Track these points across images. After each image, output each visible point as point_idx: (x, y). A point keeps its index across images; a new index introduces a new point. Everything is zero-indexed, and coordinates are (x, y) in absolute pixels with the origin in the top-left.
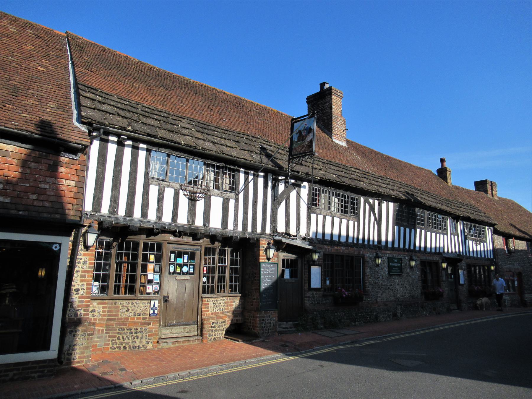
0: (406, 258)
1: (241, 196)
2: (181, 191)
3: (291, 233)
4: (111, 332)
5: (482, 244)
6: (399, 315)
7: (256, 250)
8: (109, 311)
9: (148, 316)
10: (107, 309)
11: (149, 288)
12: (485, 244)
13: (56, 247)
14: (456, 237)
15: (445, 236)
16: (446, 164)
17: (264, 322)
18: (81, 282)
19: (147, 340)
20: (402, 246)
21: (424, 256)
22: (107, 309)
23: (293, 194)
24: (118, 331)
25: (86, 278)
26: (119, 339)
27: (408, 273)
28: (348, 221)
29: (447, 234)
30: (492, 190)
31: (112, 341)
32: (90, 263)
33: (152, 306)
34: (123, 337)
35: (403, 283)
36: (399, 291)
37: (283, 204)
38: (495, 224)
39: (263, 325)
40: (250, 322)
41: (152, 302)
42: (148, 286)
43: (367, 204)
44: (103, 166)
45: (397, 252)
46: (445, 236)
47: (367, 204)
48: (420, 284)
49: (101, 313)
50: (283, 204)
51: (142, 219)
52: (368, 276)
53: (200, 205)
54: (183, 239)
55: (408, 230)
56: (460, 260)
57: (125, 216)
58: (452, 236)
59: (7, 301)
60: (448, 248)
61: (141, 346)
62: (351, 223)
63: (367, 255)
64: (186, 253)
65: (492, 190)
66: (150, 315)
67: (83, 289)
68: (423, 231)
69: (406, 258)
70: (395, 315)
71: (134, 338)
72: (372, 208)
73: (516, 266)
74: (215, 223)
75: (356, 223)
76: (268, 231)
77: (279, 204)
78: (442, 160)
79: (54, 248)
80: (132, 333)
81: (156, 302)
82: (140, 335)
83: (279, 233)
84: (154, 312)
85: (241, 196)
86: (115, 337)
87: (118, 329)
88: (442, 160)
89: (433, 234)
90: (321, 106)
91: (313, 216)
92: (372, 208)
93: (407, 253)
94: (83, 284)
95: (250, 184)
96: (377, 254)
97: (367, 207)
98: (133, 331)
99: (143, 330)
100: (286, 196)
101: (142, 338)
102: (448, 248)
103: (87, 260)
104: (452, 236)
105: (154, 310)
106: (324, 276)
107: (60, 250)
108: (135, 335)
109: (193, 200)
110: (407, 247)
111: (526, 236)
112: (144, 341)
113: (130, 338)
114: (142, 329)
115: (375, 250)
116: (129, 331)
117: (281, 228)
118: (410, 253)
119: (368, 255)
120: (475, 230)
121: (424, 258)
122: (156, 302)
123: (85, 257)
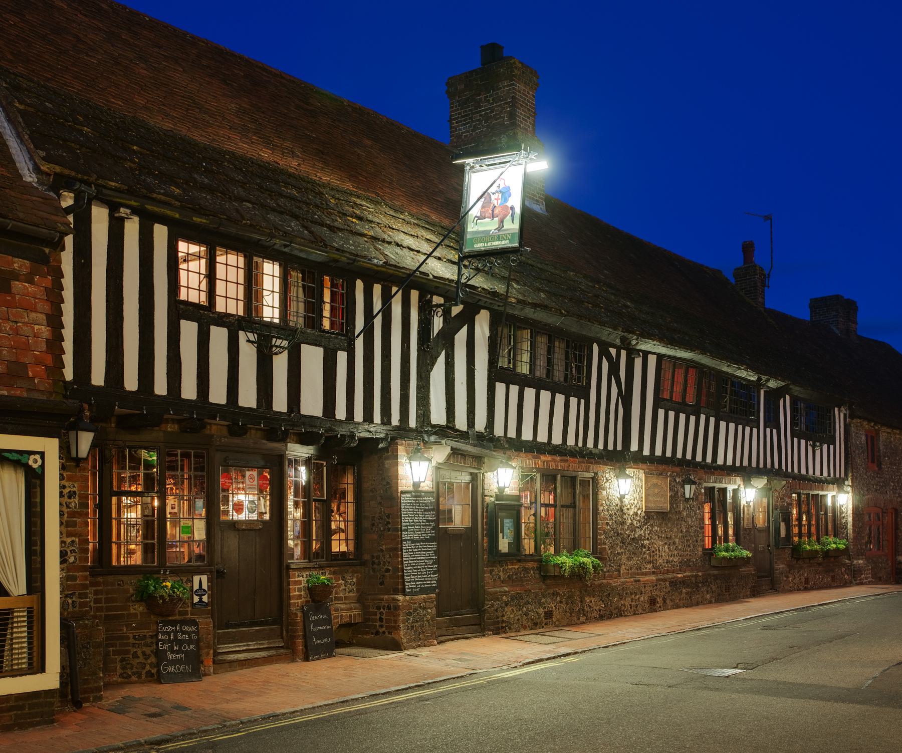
1: (359, 344)
3: (457, 427)
4: (118, 642)
7: (387, 463)
8: (108, 600)
9: (189, 609)
10: (103, 597)
12: (832, 447)
15: (755, 430)
16: (760, 259)
18: (68, 536)
22: (103, 597)
23: (461, 336)
24: (132, 641)
26: (135, 656)
27: (680, 513)
29: (584, 394)
30: (222, 540)
31: (122, 660)
34: (144, 653)
37: (441, 360)
40: (381, 620)
41: (196, 579)
43: (604, 359)
44: (653, 602)
46: (755, 430)
47: (604, 359)
49: (92, 604)
50: (441, 360)
52: (604, 519)
54: (416, 663)
55: (740, 427)
58: (796, 440)
59: (861, 562)
62: (573, 401)
64: (119, 474)
65: (222, 540)
66: (193, 605)
68: (712, 420)
72: (614, 370)
75: (582, 401)
78: (748, 249)
79: (31, 462)
81: (204, 579)
83: (434, 426)
85: (359, 344)
86: (128, 652)
87: (131, 636)
88: (748, 249)
89: (732, 426)
90: (485, 106)
91: (500, 387)
92: (614, 370)
94: (73, 542)
95: (393, 300)
97: (605, 365)
100: (447, 339)
102: (550, 351)
105: (201, 596)
107: (42, 466)
111: (521, 638)
120: (96, 593)
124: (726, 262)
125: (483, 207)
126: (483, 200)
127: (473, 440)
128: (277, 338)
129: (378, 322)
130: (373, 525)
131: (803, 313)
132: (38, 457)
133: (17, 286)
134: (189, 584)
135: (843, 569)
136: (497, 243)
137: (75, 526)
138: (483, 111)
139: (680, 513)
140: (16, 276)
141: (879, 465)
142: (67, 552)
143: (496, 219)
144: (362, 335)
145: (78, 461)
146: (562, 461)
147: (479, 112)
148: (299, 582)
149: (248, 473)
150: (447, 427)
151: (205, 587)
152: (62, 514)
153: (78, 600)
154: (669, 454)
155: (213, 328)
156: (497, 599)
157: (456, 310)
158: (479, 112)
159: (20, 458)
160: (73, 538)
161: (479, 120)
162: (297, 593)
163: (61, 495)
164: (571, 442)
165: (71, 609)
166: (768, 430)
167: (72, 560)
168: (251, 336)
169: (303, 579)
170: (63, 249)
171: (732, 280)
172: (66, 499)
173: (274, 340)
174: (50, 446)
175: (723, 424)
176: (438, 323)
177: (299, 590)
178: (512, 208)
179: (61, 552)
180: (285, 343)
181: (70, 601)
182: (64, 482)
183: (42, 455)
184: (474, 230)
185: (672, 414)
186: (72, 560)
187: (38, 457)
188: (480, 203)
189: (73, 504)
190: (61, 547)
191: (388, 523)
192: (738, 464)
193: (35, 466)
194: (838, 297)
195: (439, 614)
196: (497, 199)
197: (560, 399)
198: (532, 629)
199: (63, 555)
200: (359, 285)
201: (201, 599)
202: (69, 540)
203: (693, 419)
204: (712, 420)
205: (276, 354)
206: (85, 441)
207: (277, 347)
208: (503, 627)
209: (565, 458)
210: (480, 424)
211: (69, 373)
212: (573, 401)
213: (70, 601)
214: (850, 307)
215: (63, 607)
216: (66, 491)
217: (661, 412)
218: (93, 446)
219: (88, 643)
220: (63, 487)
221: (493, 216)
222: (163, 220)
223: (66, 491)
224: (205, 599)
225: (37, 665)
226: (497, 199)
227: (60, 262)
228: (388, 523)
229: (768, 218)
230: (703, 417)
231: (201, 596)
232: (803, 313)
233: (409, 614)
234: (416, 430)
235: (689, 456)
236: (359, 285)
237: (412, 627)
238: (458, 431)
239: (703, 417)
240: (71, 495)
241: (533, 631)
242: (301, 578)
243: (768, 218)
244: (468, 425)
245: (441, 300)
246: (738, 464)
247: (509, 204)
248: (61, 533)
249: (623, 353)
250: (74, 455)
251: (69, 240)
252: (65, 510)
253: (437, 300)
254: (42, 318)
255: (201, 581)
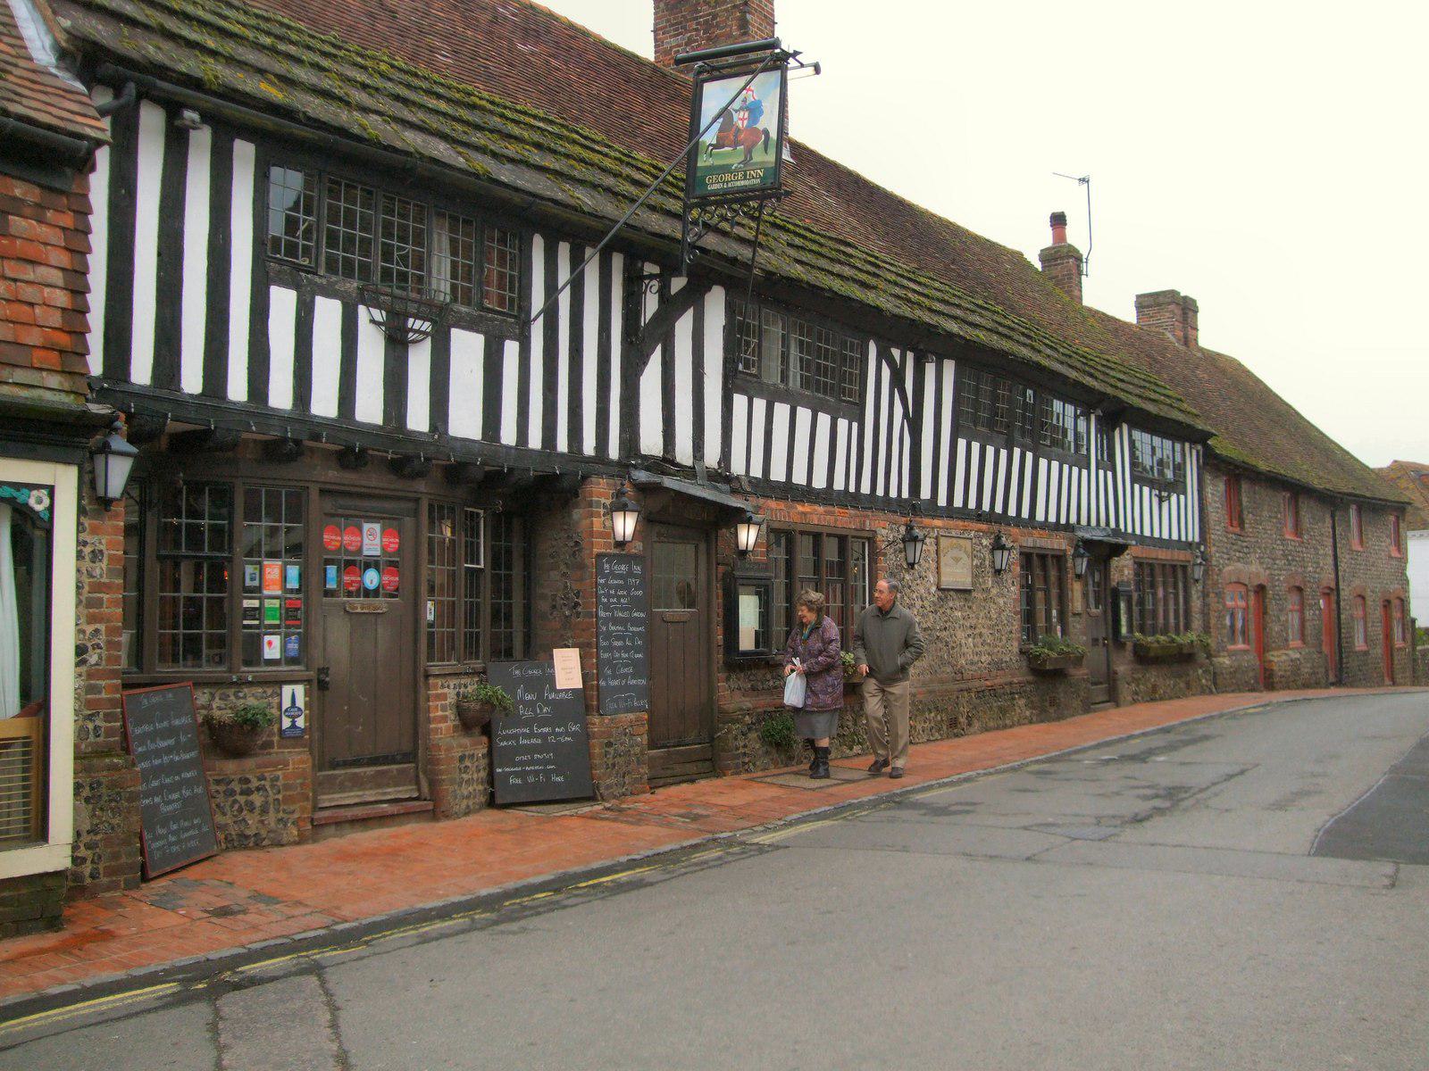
0: (985, 542)
2: (362, 309)
3: (678, 460)
5: (1174, 498)
6: (963, 720)
9: (276, 739)
11: (270, 643)
12: (1182, 497)
13: (40, 501)
14: (1109, 474)
15: (1084, 472)
16: (1075, 236)
17: (611, 750)
18: (89, 623)
19: (281, 815)
20: (972, 505)
21: (1031, 535)
23: (683, 327)
25: (105, 610)
27: (988, 591)
28: (1126, 529)
32: (111, 558)
33: (286, 703)
35: (973, 622)
36: (964, 649)
38: (1211, 435)
39: (610, 762)
42: (267, 638)
45: (960, 523)
46: (1084, 472)
48: (1016, 625)
51: (252, 407)
53: (419, 362)
56: (1118, 550)
57: (202, 395)
58: (1101, 472)
60: (1126, 526)
61: (264, 833)
62: (843, 424)
63: (884, 532)
67: (99, 646)
68: (1029, 455)
69: (985, 542)
70: (953, 723)
71: (241, 810)
72: (897, 380)
73: (1255, 568)
74: (465, 422)
75: (855, 425)
76: (614, 452)
77: (643, 361)
78: (1058, 221)
79: (32, 502)
80: (233, 793)
81: (300, 690)
82: (257, 799)
83: (646, 457)
84: (293, 725)
88: (1058, 221)
91: (740, 401)
93: (984, 527)
94: (97, 631)
96: (910, 528)
98: (237, 787)
99: (267, 784)
101: (264, 811)
102: (1126, 526)
103: (103, 547)
104: (1101, 472)
105: (293, 718)
106: (223, 576)
107: (51, 509)
108: (242, 799)
109: (397, 344)
110: (958, 503)
112: (271, 818)
113: (227, 808)
114: (262, 778)
115: (903, 515)
116: (221, 788)
117: (651, 442)
118: (996, 527)
119: (886, 529)
121: (1029, 542)
122: (300, 690)
123: (95, 539)
124: (1031, 243)
125: (721, 130)
126: (721, 120)
127: (702, 478)
128: (417, 317)
129: (564, 300)
130: (554, 607)
131: (1129, 315)
132: (44, 492)
133: (18, 224)
134: (276, 700)
135: (1200, 671)
136: (743, 183)
137: (329, 246)
138: (701, 17)
139: (988, 591)
140: (16, 207)
141: (1242, 524)
142: (87, 648)
143: (741, 148)
144: (569, 287)
145: (105, 503)
146: (827, 513)
147: (696, 18)
148: (444, 697)
149: (366, 526)
150: (664, 459)
151: (300, 703)
152: (79, 588)
153: (103, 724)
154: (972, 505)
155: (319, 300)
156: (737, 721)
157: (678, 284)
158: (696, 18)
159: (16, 494)
160: (97, 626)
161: (696, 30)
162: (440, 713)
163: (80, 556)
164: (839, 485)
165: (92, 738)
166: (283, 301)
167: (93, 659)
168: (378, 315)
169: (451, 694)
170: (93, 168)
171: (1038, 266)
172: (87, 564)
173: (411, 320)
174: (65, 479)
175: (1043, 463)
176: (651, 304)
177: (444, 708)
178: (766, 133)
179: (77, 647)
180: (427, 326)
181: (91, 726)
182: (83, 536)
183: (51, 490)
184: (707, 164)
185: (976, 446)
186: (93, 659)
187: (44, 492)
188: (717, 126)
189: (98, 572)
190: (77, 638)
191: (577, 604)
192: (1063, 521)
193: (39, 508)
194: (1173, 293)
195: (653, 744)
196: (743, 119)
197: (804, 415)
198: (786, 766)
199: (80, 651)
200: (538, 244)
201: (293, 722)
202: (90, 629)
203: (1003, 453)
204: (1029, 455)
205: (415, 342)
206: (117, 474)
207: (416, 331)
208: (744, 763)
209: (831, 508)
210: (712, 456)
211: (95, 364)
212: (843, 424)
213: (91, 726)
214: (1185, 309)
215: (81, 734)
216: (87, 550)
217: (962, 443)
218: (133, 479)
219: (118, 793)
220: (81, 543)
221: (735, 144)
222: (249, 133)
223: (87, 550)
224: (301, 722)
225: (38, 832)
226: (743, 119)
227: (87, 188)
228: (577, 604)
229: (1084, 180)
230: (1017, 451)
231: (293, 718)
232: (1129, 315)
233: (609, 744)
234: (619, 463)
235: (999, 509)
236: (538, 244)
237: (614, 765)
238: (678, 465)
239: (1017, 451)
240: (96, 555)
241: (787, 769)
242: (446, 690)
243: (1084, 180)
244: (695, 457)
245: (656, 270)
246: (1063, 521)
247: (760, 126)
248: (78, 618)
249: (910, 356)
250: (101, 493)
251: (103, 157)
252: (86, 580)
253: (650, 268)
254: (57, 277)
255: (295, 694)
